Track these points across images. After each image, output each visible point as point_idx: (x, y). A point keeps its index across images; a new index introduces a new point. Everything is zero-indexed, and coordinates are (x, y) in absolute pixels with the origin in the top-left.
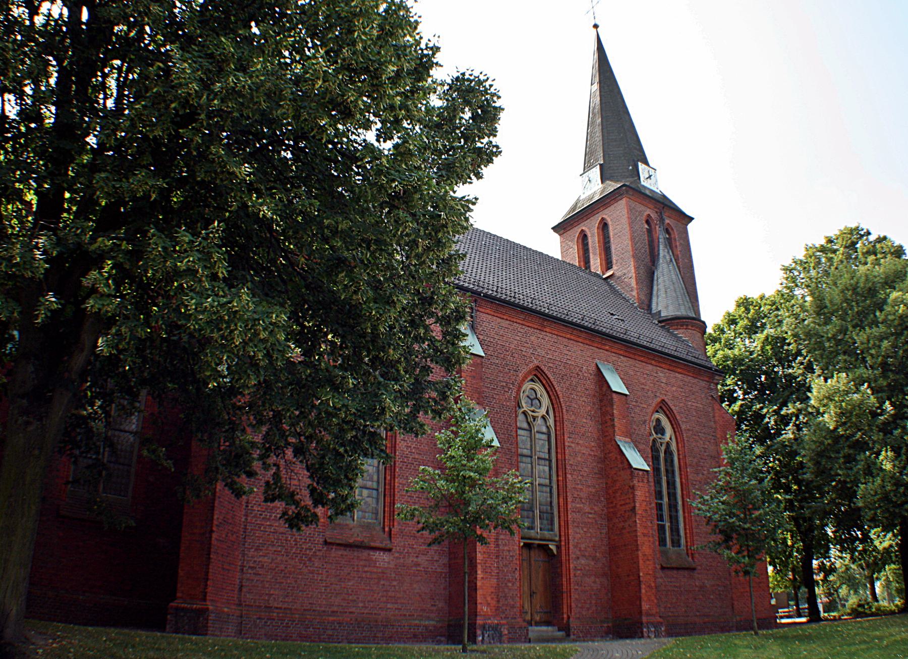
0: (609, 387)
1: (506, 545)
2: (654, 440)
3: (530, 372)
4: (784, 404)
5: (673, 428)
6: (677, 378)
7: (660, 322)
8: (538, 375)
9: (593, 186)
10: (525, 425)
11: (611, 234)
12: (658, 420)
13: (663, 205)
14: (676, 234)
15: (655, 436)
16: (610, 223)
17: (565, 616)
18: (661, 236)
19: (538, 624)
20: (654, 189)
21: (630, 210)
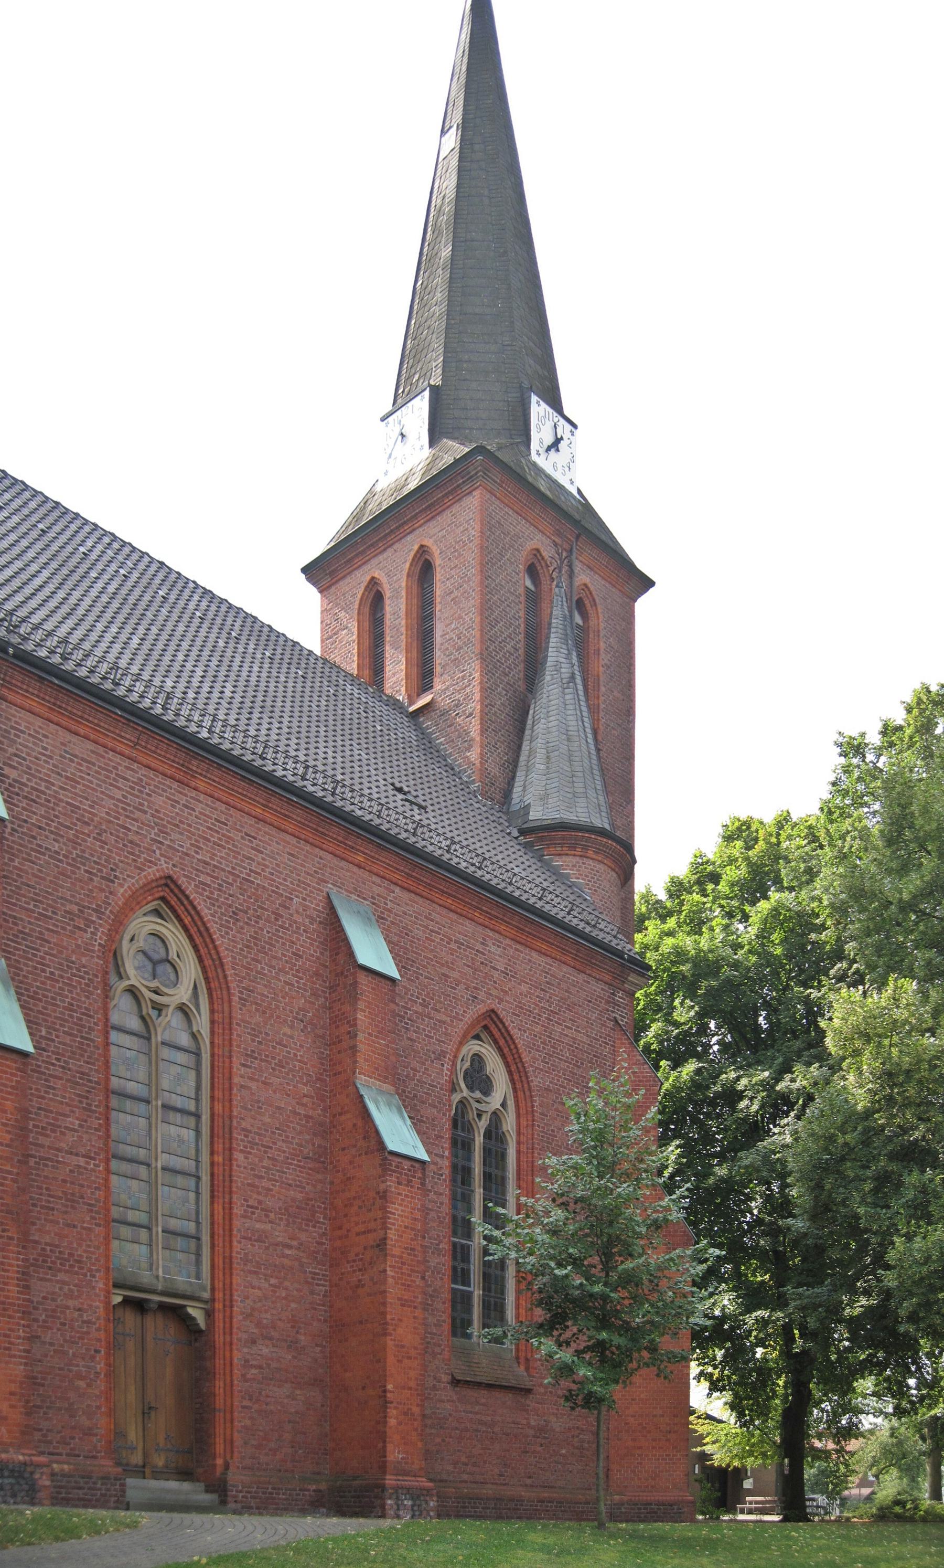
0: (351, 954)
1: (70, 1296)
2: (463, 1103)
3: (148, 888)
4: (786, 1068)
5: (512, 1081)
6: (534, 963)
7: (523, 832)
8: (170, 898)
9: (401, 452)
10: (134, 1023)
11: (439, 591)
12: (478, 1059)
13: (579, 527)
14: (601, 620)
15: (466, 1093)
16: (438, 561)
17: (219, 1461)
18: (558, 612)
19: (157, 1474)
20: (564, 481)
21: (489, 526)
